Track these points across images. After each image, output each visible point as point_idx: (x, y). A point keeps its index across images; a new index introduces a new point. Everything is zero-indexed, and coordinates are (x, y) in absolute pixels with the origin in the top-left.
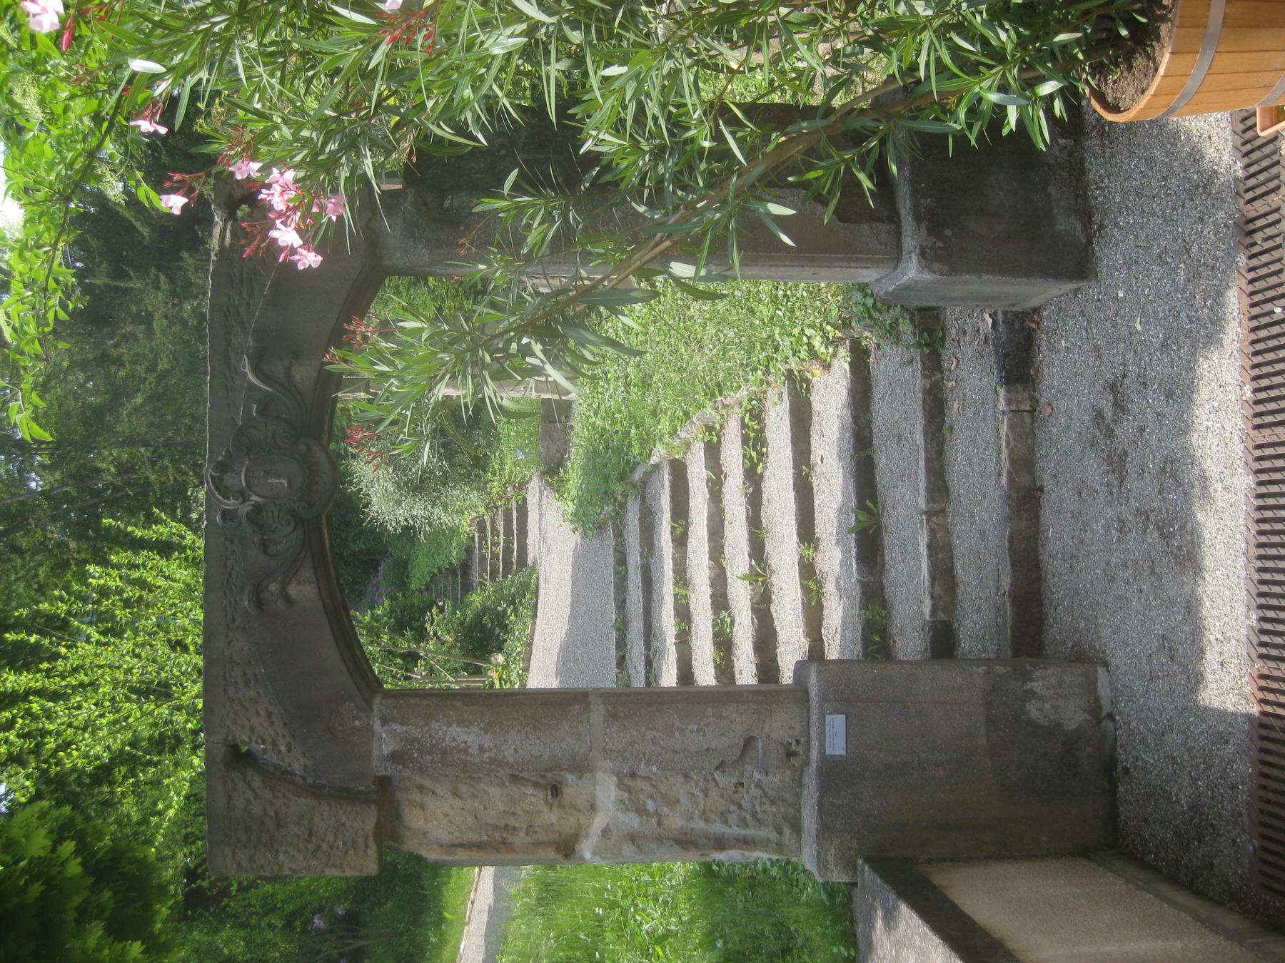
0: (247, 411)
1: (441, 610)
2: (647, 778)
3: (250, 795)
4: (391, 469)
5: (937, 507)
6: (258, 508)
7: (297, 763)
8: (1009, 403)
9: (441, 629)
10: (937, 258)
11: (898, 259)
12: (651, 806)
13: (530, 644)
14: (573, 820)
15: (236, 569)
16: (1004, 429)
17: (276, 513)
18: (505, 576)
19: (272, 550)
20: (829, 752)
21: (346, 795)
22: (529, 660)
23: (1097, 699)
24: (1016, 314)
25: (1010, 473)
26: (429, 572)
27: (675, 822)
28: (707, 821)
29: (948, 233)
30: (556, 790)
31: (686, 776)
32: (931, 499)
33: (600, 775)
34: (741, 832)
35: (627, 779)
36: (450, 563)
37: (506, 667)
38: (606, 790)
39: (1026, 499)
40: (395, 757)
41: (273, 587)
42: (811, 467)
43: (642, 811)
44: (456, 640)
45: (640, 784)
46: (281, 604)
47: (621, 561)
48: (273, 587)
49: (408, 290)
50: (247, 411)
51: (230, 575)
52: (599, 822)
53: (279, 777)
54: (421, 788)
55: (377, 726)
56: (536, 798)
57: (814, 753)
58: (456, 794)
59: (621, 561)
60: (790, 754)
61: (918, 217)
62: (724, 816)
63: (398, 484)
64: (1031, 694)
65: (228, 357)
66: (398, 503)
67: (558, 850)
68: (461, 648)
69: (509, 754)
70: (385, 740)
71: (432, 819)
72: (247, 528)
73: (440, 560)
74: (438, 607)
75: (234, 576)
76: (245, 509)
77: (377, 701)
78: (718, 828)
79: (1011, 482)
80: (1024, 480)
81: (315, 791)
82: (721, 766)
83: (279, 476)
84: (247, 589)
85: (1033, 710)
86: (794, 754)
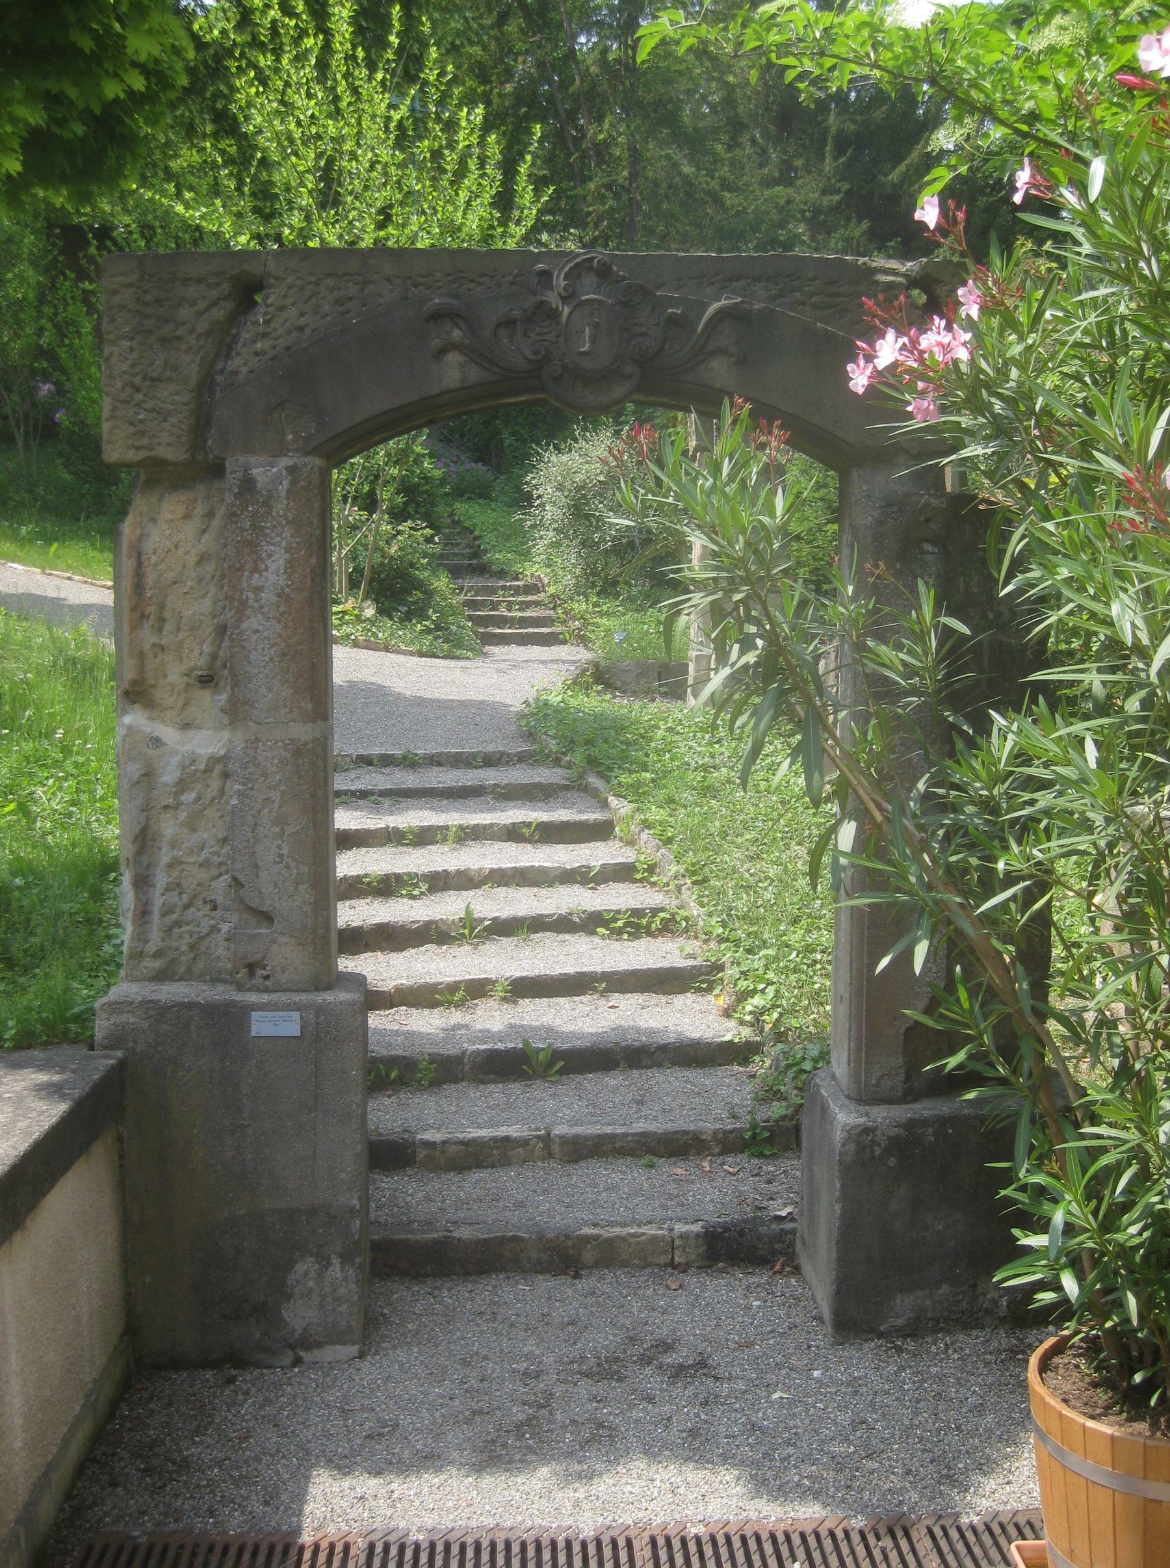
0: (673, 302)
1: (429, 540)
2: (222, 792)
4: (601, 478)
5: (556, 1148)
6: (554, 315)
7: (240, 363)
8: (684, 1236)
9: (406, 540)
10: (861, 1149)
11: (860, 1100)
12: (189, 797)
13: (386, 649)
15: (480, 289)
16: (651, 1231)
17: (547, 337)
18: (470, 618)
19: (503, 333)
20: (255, 1015)
21: (201, 422)
22: (368, 648)
23: (320, 1345)
24: (792, 1245)
26: (475, 525)
27: (169, 827)
28: (170, 866)
29: (892, 1162)
30: (207, 681)
31: (225, 840)
32: (565, 1140)
33: (226, 735)
36: (486, 551)
37: (359, 619)
38: (207, 743)
39: (565, 1257)
40: (248, 484)
41: (457, 334)
42: (604, 993)
43: (182, 786)
44: (392, 558)
45: (215, 783)
46: (436, 343)
47: (489, 761)
49: (822, 499)
50: (673, 302)
51: (472, 281)
52: (168, 734)
53: (224, 340)
54: (210, 515)
56: (197, 657)
57: (252, 998)
58: (202, 558)
60: (252, 968)
62: (176, 886)
63: (583, 488)
64: (325, 1263)
65: (739, 279)
66: (560, 488)
68: (382, 564)
69: (252, 623)
70: (268, 471)
71: (172, 529)
72: (531, 301)
73: (490, 538)
74: (432, 536)
75: (471, 285)
76: (553, 299)
77: (317, 462)
78: (161, 880)
79: (586, 1239)
80: (588, 1256)
81: (206, 385)
82: (237, 883)
83: (593, 341)
84: (454, 302)
85: (305, 1266)
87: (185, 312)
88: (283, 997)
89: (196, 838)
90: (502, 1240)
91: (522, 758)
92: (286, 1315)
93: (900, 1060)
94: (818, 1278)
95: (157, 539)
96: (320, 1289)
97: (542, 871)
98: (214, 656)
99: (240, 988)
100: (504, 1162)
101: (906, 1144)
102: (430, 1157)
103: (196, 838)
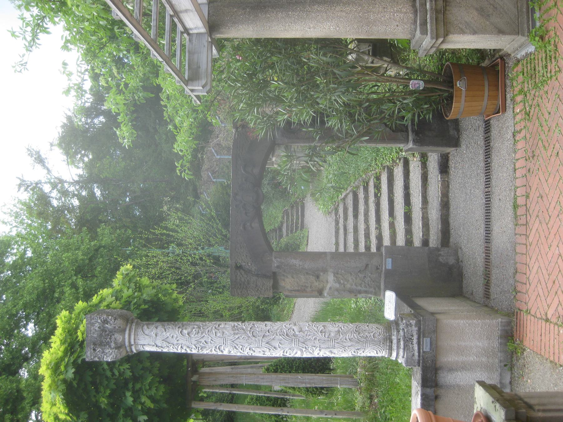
2: (341, 274)
3: (241, 276)
5: (425, 207)
7: (254, 268)
8: (441, 178)
10: (417, 142)
11: (408, 142)
12: (342, 281)
14: (322, 285)
16: (440, 185)
18: (296, 232)
20: (387, 268)
21: (265, 276)
23: (458, 257)
24: (444, 154)
25: (441, 198)
27: (348, 286)
28: (356, 286)
29: (421, 135)
30: (318, 277)
31: (351, 274)
32: (423, 204)
33: (329, 273)
34: (365, 289)
35: (336, 274)
38: (331, 278)
39: (445, 205)
40: (278, 267)
41: (248, 224)
42: (393, 195)
43: (340, 283)
45: (339, 276)
47: (337, 223)
48: (248, 224)
52: (329, 286)
53: (248, 272)
54: (284, 275)
55: (274, 259)
56: (312, 278)
57: (384, 268)
58: (293, 277)
59: (337, 223)
60: (377, 269)
61: (413, 131)
62: (361, 285)
64: (440, 255)
67: (318, 292)
69: (306, 266)
70: (275, 263)
71: (287, 283)
77: (274, 253)
78: (359, 288)
79: (441, 200)
80: (445, 199)
81: (257, 275)
82: (360, 271)
85: (441, 259)
86: (379, 269)
87: (243, 280)
88: (384, 262)
89: (350, 280)
90: (441, 218)
91: (336, 214)
92: (451, 263)
93: (399, 133)
94: (450, 150)
95: (288, 287)
96: (446, 257)
97: (365, 210)
98: (313, 275)
99: (382, 271)
100: (427, 219)
101: (416, 133)
102: (426, 235)
103: (350, 280)
